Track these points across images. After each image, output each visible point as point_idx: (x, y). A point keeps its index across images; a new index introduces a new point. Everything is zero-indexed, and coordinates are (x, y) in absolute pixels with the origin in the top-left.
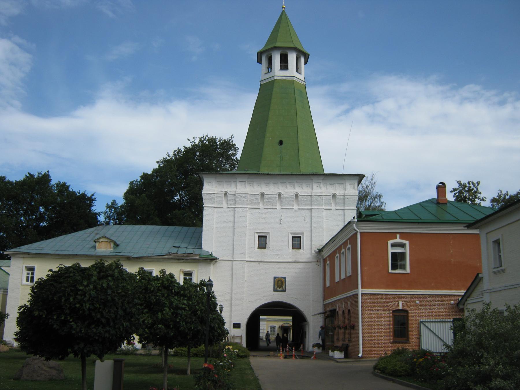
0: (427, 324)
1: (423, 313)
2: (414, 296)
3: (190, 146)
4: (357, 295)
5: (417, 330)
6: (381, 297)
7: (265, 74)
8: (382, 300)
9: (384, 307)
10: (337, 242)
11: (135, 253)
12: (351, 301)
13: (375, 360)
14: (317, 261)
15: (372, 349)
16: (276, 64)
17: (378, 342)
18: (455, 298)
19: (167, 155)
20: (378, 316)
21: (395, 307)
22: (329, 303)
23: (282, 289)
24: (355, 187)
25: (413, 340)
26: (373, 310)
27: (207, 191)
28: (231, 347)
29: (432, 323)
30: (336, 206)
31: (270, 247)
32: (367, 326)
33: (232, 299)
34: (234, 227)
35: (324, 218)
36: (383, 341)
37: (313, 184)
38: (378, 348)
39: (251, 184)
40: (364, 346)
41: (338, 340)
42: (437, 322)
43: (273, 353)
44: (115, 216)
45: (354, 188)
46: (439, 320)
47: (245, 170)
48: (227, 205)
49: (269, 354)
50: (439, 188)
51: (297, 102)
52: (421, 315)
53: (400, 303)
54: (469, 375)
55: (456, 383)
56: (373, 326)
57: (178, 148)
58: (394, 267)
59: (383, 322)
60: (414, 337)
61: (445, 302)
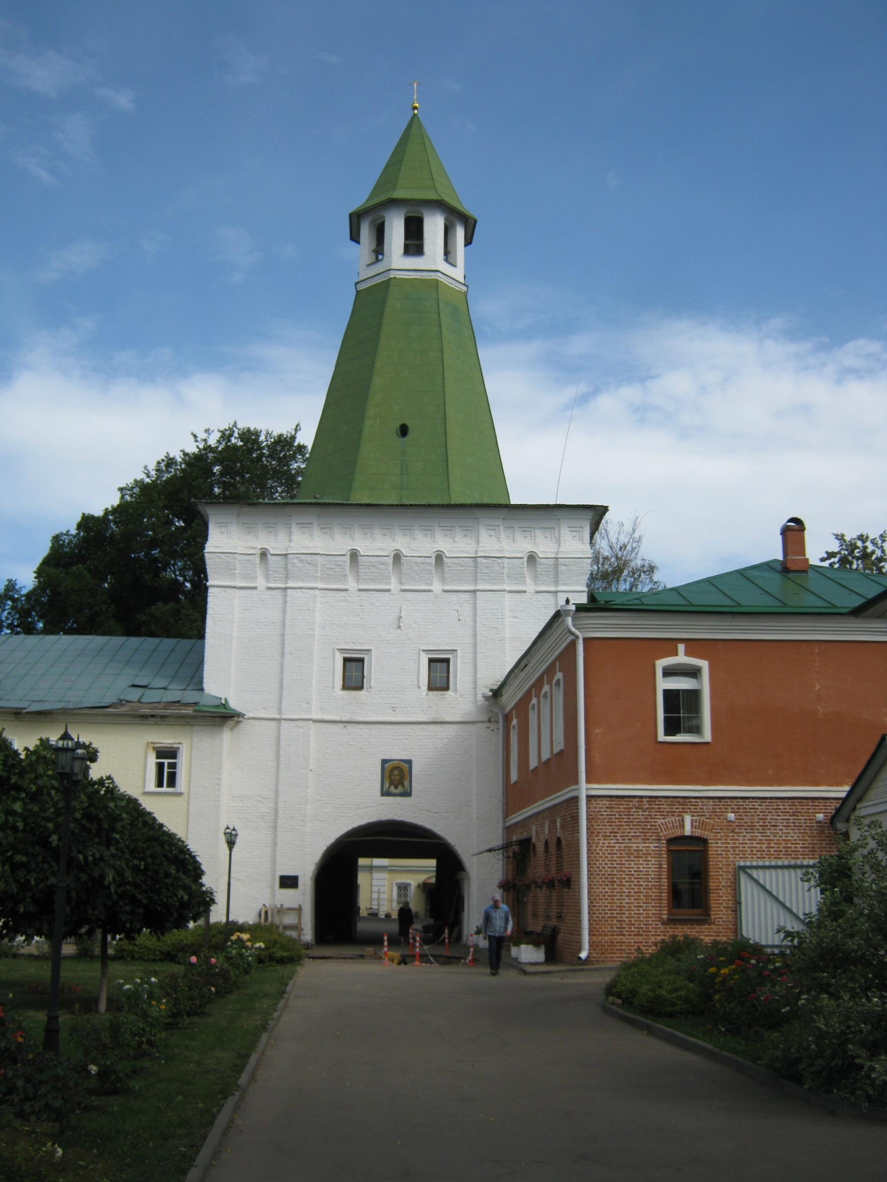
0: (754, 873)
1: (746, 846)
2: (723, 800)
3: (196, 451)
4: (575, 800)
5: (729, 889)
6: (637, 804)
7: (368, 265)
8: (640, 813)
9: (645, 829)
10: (532, 668)
11: (33, 701)
12: (562, 815)
13: (611, 969)
14: (490, 721)
15: (616, 939)
16: (393, 243)
17: (631, 921)
18: (826, 806)
19: (145, 473)
20: (629, 854)
21: (670, 831)
22: (516, 824)
23: (402, 790)
24: (584, 538)
25: (720, 914)
26: (618, 838)
27: (217, 547)
28: (245, 936)
29: (767, 872)
30: (536, 584)
31: (372, 685)
32: (600, 880)
33: (276, 814)
34: (283, 635)
35: (508, 614)
36: (644, 917)
37: (479, 529)
38: (630, 935)
39: (325, 531)
40: (592, 931)
41: (535, 916)
42: (782, 867)
43: (372, 949)
44: (14, 619)
45: (581, 540)
46: (786, 863)
47: (315, 498)
48: (268, 581)
49: (364, 953)
50: (788, 533)
51: (445, 332)
52: (741, 849)
53: (688, 819)
54: (851, 1023)
55: (813, 1046)
56: (618, 878)
57: (166, 455)
58: (672, 727)
59: (643, 868)
60: (724, 907)
61: (802, 816)
